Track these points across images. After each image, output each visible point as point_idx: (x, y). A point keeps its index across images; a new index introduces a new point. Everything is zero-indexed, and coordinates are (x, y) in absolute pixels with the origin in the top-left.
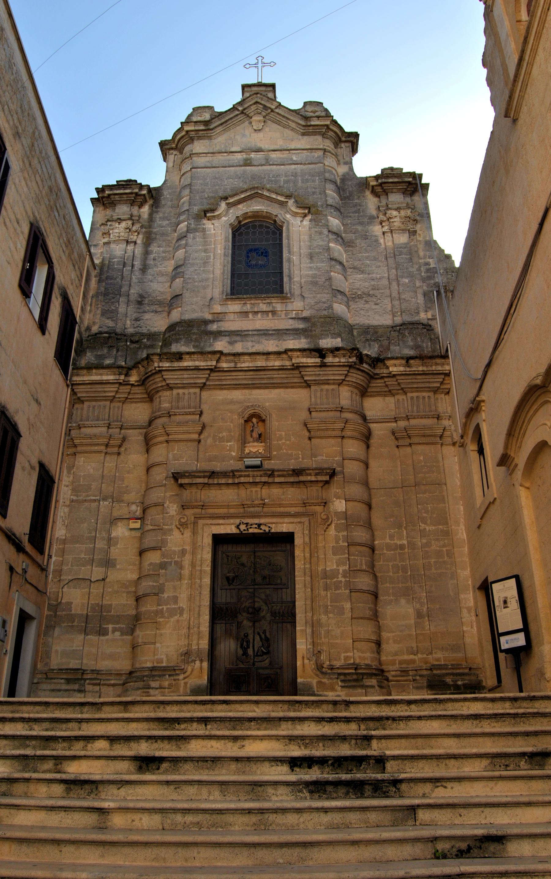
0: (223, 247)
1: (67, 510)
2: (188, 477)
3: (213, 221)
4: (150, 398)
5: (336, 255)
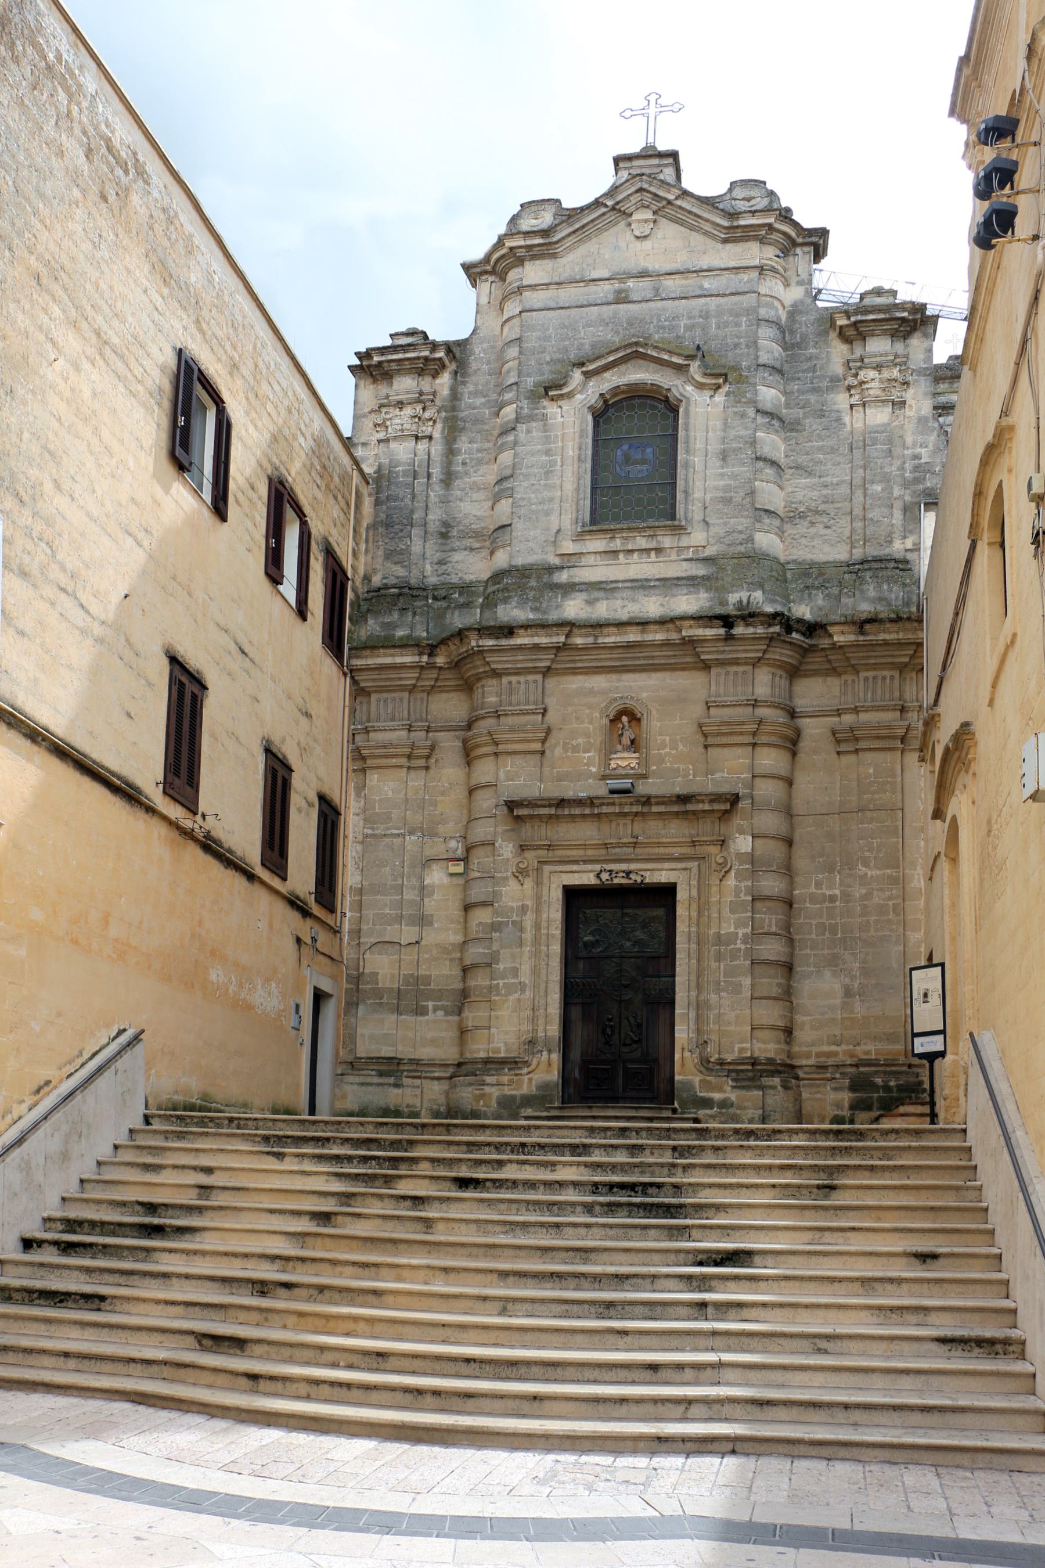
0: (576, 446)
1: (359, 848)
2: (527, 806)
3: (560, 403)
4: (468, 687)
5: (766, 451)
